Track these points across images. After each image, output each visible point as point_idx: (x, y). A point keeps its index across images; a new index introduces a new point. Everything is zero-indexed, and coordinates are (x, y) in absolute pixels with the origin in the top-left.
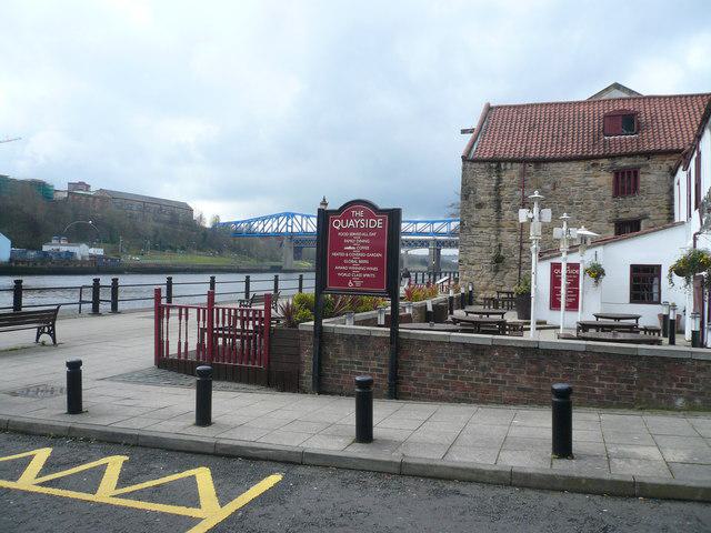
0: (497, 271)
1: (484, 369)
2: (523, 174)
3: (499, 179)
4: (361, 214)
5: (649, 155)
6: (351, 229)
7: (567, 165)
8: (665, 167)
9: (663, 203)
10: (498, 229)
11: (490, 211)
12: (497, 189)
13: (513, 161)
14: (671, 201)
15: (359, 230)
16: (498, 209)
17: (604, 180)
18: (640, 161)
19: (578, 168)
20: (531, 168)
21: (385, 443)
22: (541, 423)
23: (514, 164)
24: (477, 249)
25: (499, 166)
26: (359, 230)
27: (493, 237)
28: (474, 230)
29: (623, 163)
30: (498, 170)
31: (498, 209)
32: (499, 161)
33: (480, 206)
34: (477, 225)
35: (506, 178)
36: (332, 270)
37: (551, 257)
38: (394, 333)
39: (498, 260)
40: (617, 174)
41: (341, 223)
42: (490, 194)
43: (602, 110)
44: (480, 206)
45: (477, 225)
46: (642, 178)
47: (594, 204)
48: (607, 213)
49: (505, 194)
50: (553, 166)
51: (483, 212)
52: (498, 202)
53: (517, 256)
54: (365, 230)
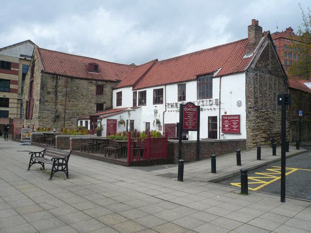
0: (55, 121)
1: (214, 148)
2: (67, 82)
3: (57, 83)
4: (191, 107)
5: (107, 81)
6: (189, 111)
7: (82, 81)
8: (111, 86)
9: (110, 98)
10: (56, 103)
11: (52, 96)
12: (56, 86)
13: (63, 76)
14: (112, 98)
15: (190, 111)
16: (56, 95)
17: (94, 88)
18: (104, 83)
19: (85, 83)
20: (69, 80)
21: (220, 172)
22: (233, 158)
23: (63, 78)
24: (47, 112)
25: (57, 77)
26: (190, 111)
27: (54, 107)
28: (45, 103)
29: (100, 83)
30: (57, 78)
31: (56, 95)
32: (57, 75)
33: (49, 93)
34: (47, 101)
35: (60, 83)
36: (185, 124)
37: (107, 117)
38: (180, 142)
39: (58, 117)
40: (97, 87)
41: (186, 109)
42: (53, 88)
43: (91, 61)
44: (49, 93)
45: (47, 101)
46: (105, 89)
47: (90, 97)
48: (94, 101)
49: (59, 89)
50: (77, 80)
51: (50, 96)
52: (56, 92)
53: (63, 115)
54: (193, 112)
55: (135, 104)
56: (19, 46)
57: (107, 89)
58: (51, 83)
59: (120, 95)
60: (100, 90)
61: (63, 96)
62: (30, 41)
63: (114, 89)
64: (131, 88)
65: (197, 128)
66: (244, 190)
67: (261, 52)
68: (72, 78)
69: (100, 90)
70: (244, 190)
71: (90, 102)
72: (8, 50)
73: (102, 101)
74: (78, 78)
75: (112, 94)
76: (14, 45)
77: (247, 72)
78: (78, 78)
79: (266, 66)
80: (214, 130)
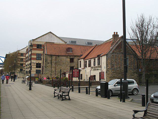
2: (56, 58)
3: (52, 59)
5: (75, 56)
7: (63, 57)
9: (77, 64)
11: (50, 64)
13: (54, 55)
16: (52, 64)
17: (69, 60)
20: (57, 57)
27: (51, 69)
29: (71, 57)
30: (52, 57)
32: (52, 55)
33: (48, 63)
35: (53, 58)
44: (48, 63)
48: (69, 65)
51: (49, 64)
55: (84, 67)
56: (45, 36)
57: (75, 60)
58: (49, 59)
59: (80, 61)
60: (72, 60)
61: (54, 64)
62: (50, 32)
63: (79, 60)
64: (83, 60)
65: (104, 79)
66: (79, 92)
67: (116, 45)
68: (58, 56)
69: (72, 60)
70: (79, 92)
71: (67, 66)
72: (40, 38)
73: (73, 65)
74: (61, 56)
75: (78, 62)
76: (43, 36)
77: (107, 55)
78: (61, 56)
79: (120, 51)
80: (38, 69)
